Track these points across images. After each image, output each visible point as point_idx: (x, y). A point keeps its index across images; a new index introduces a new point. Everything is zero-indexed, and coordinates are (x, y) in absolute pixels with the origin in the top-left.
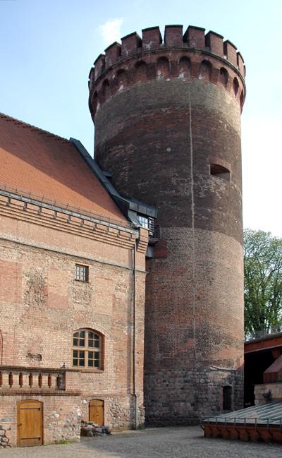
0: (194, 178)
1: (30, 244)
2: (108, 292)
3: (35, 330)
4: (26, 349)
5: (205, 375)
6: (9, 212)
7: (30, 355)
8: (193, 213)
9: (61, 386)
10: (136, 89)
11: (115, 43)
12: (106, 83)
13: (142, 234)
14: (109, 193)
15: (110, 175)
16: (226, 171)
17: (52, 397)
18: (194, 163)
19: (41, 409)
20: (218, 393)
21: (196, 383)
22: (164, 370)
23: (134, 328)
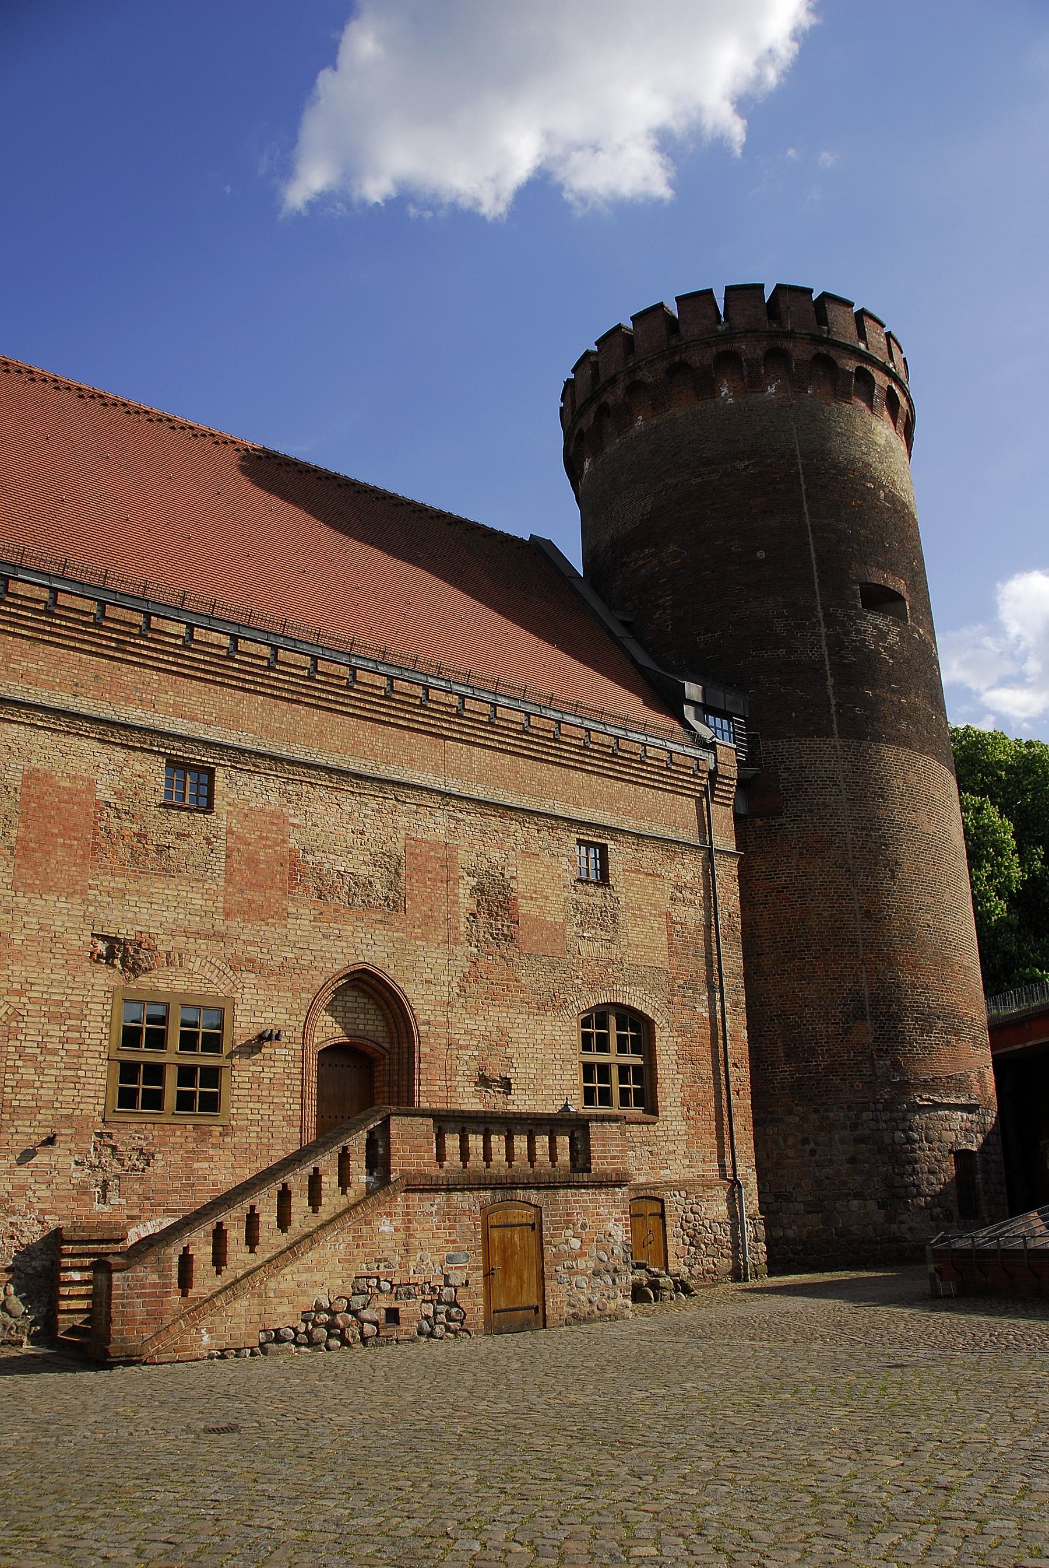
1: (474, 794)
2: (655, 906)
3: (494, 1013)
4: (475, 1065)
6: (425, 720)
7: (484, 1081)
8: (833, 702)
9: (579, 1163)
11: (619, 327)
12: (603, 411)
13: (720, 759)
14: (633, 661)
15: (629, 619)
16: (898, 598)
17: (562, 1192)
19: (536, 1226)
23: (722, 1000)
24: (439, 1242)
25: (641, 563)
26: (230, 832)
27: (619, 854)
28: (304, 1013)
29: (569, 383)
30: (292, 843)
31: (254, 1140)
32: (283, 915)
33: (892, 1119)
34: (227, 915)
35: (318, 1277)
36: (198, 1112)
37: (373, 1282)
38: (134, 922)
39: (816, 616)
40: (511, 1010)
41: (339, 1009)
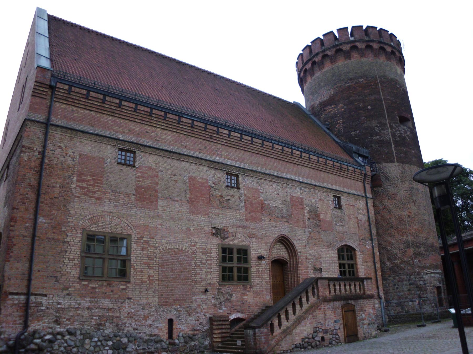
4: (313, 265)
5: (423, 277)
7: (315, 269)
8: (394, 152)
10: (338, 67)
12: (314, 63)
18: (388, 116)
20: (434, 292)
24: (332, 317)
25: (331, 110)
26: (245, 195)
29: (297, 63)
30: (261, 198)
32: (261, 220)
34: (247, 220)
35: (305, 328)
37: (317, 329)
38: (222, 223)
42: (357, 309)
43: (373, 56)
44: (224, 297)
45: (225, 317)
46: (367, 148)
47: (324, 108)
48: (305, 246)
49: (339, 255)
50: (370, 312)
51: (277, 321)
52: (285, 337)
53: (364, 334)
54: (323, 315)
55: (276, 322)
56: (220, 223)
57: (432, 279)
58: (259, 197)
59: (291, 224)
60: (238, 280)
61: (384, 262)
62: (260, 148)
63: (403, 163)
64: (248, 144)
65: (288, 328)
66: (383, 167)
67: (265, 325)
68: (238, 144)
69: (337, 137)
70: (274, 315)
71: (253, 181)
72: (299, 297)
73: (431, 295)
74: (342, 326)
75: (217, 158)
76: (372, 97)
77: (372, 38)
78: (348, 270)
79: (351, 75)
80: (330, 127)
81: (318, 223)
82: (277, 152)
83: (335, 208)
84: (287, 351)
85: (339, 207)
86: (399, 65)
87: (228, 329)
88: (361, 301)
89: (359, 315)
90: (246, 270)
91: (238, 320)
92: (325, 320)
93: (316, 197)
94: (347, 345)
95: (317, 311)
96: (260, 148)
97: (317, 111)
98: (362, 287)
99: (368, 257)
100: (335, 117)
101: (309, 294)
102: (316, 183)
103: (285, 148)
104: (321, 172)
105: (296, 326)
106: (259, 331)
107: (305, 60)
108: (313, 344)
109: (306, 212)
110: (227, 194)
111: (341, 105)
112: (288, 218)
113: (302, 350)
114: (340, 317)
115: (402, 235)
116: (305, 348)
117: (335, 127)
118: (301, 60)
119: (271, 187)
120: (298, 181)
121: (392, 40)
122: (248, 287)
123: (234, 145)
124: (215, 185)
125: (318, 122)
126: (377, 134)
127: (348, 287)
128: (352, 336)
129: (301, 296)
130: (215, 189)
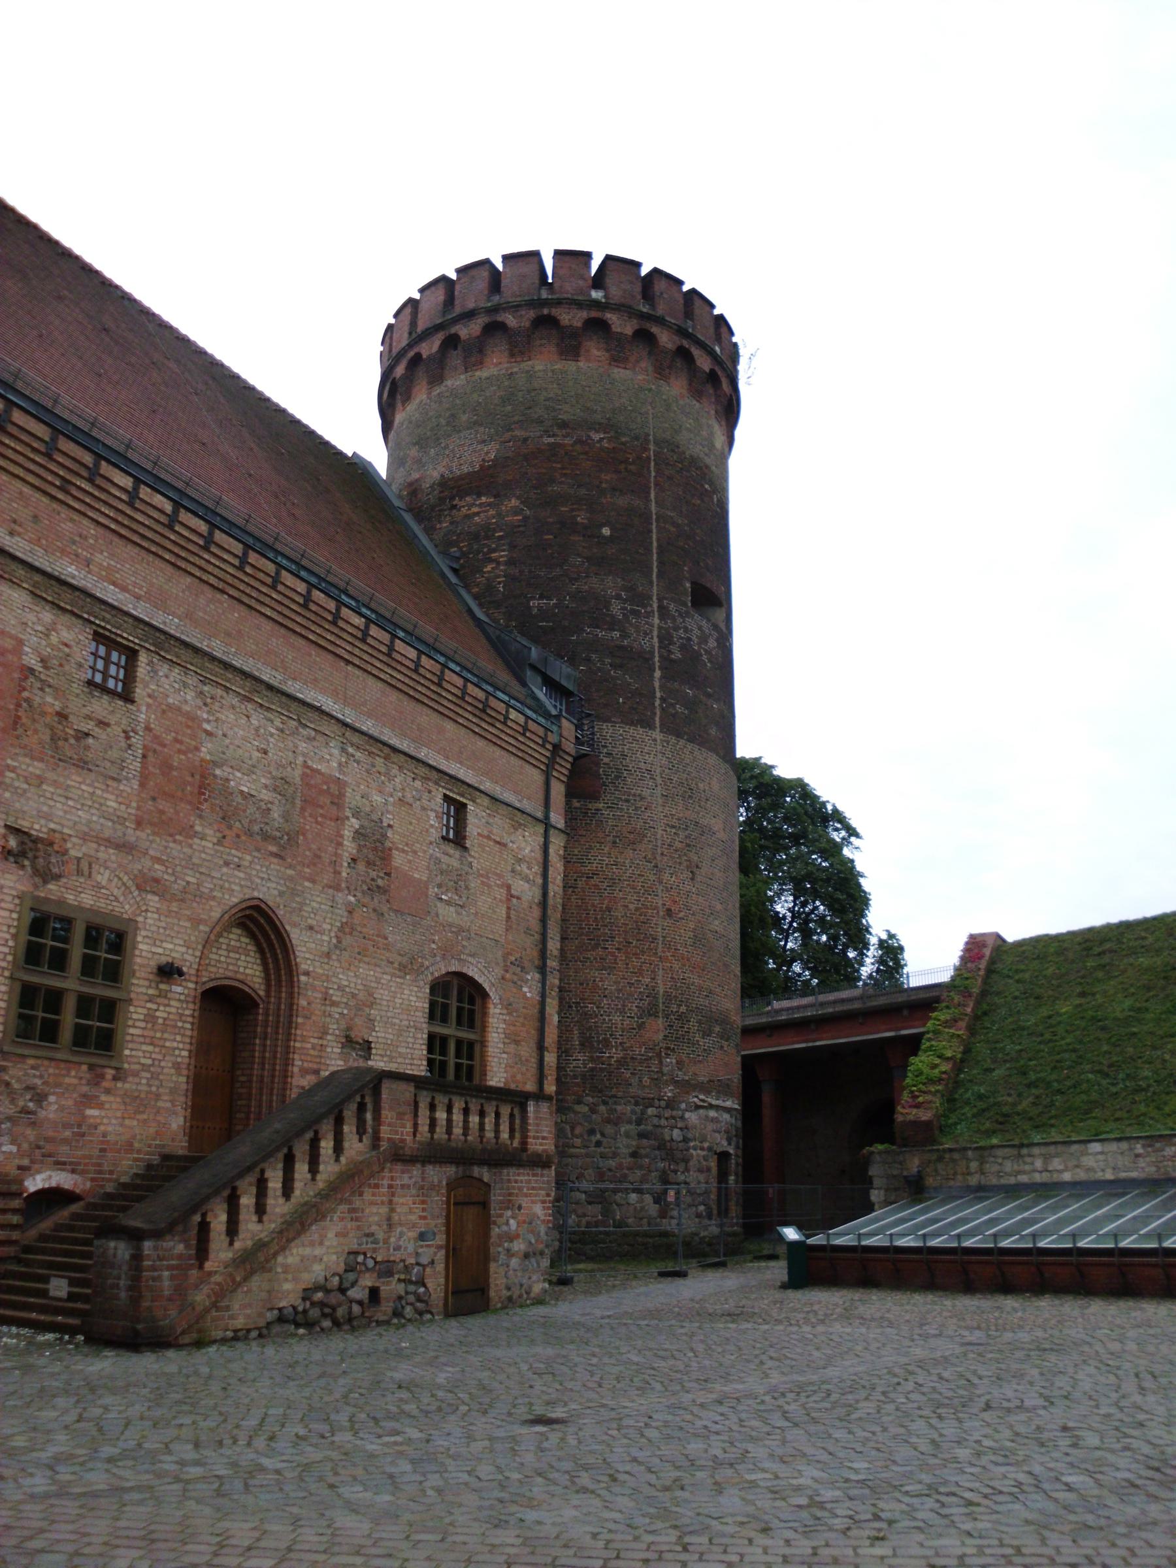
0: (659, 607)
4: (343, 1026)
5: (682, 1118)
7: (349, 1042)
8: (658, 695)
10: (530, 375)
12: (451, 342)
18: (661, 575)
20: (709, 1170)
21: (663, 1139)
22: (590, 1099)
24: (413, 1218)
25: (475, 510)
26: (148, 729)
27: (477, 818)
28: (200, 947)
29: (390, 327)
30: (204, 753)
31: (145, 1088)
32: (189, 832)
33: (673, 1118)
34: (139, 824)
35: (318, 1251)
36: (92, 1050)
37: (360, 1258)
38: (48, 817)
39: (651, 606)
40: (378, 969)
41: (224, 947)
42: (496, 1197)
43: (650, 369)
44: (13, 1101)
45: (9, 1183)
46: (573, 661)
47: (452, 498)
48: (328, 955)
49: (432, 1005)
50: (535, 1216)
51: (224, 1217)
52: (246, 1279)
53: (509, 1289)
54: (384, 1210)
55: (218, 1221)
56: (41, 815)
57: (711, 1126)
58: (197, 749)
59: (290, 867)
60: (75, 1044)
61: (566, 1051)
62: (231, 570)
63: (679, 735)
64: (191, 547)
65: (260, 1245)
66: (609, 732)
67: (180, 1228)
68: (158, 539)
69: (481, 605)
70: (217, 1192)
71: (185, 685)
72: (309, 1135)
73: (698, 1176)
74: (442, 1253)
75: (71, 569)
76: (622, 501)
77: (661, 310)
78: (453, 1064)
79: (568, 413)
80: (463, 566)
81: (380, 882)
82: (286, 602)
83: (443, 837)
84: (248, 1331)
85: (457, 838)
86: (723, 423)
87: (14, 1227)
88: (510, 1173)
89: (500, 1221)
90: (110, 1009)
91: (53, 1197)
92: (390, 1226)
93: (389, 788)
94: (453, 1323)
95: (368, 1195)
96: (231, 570)
97: (434, 502)
98: (520, 1126)
99: (523, 1025)
100: (487, 538)
101: (346, 1128)
102: (395, 741)
103: (317, 595)
104: (419, 707)
105: (289, 1241)
106: (156, 1248)
107: (421, 326)
108: (340, 1312)
109: (347, 833)
110: (85, 711)
111: (514, 502)
112: (282, 844)
113: (301, 1331)
114: (437, 1223)
115: (640, 972)
116: (310, 1325)
117: (481, 571)
118: (407, 322)
119: (243, 721)
120: (338, 720)
121: (718, 339)
122: (109, 1077)
123: (143, 537)
124: (46, 668)
125: (425, 541)
126: (612, 625)
127: (474, 1119)
128: (469, 1295)
129: (316, 1132)
130: (44, 685)
